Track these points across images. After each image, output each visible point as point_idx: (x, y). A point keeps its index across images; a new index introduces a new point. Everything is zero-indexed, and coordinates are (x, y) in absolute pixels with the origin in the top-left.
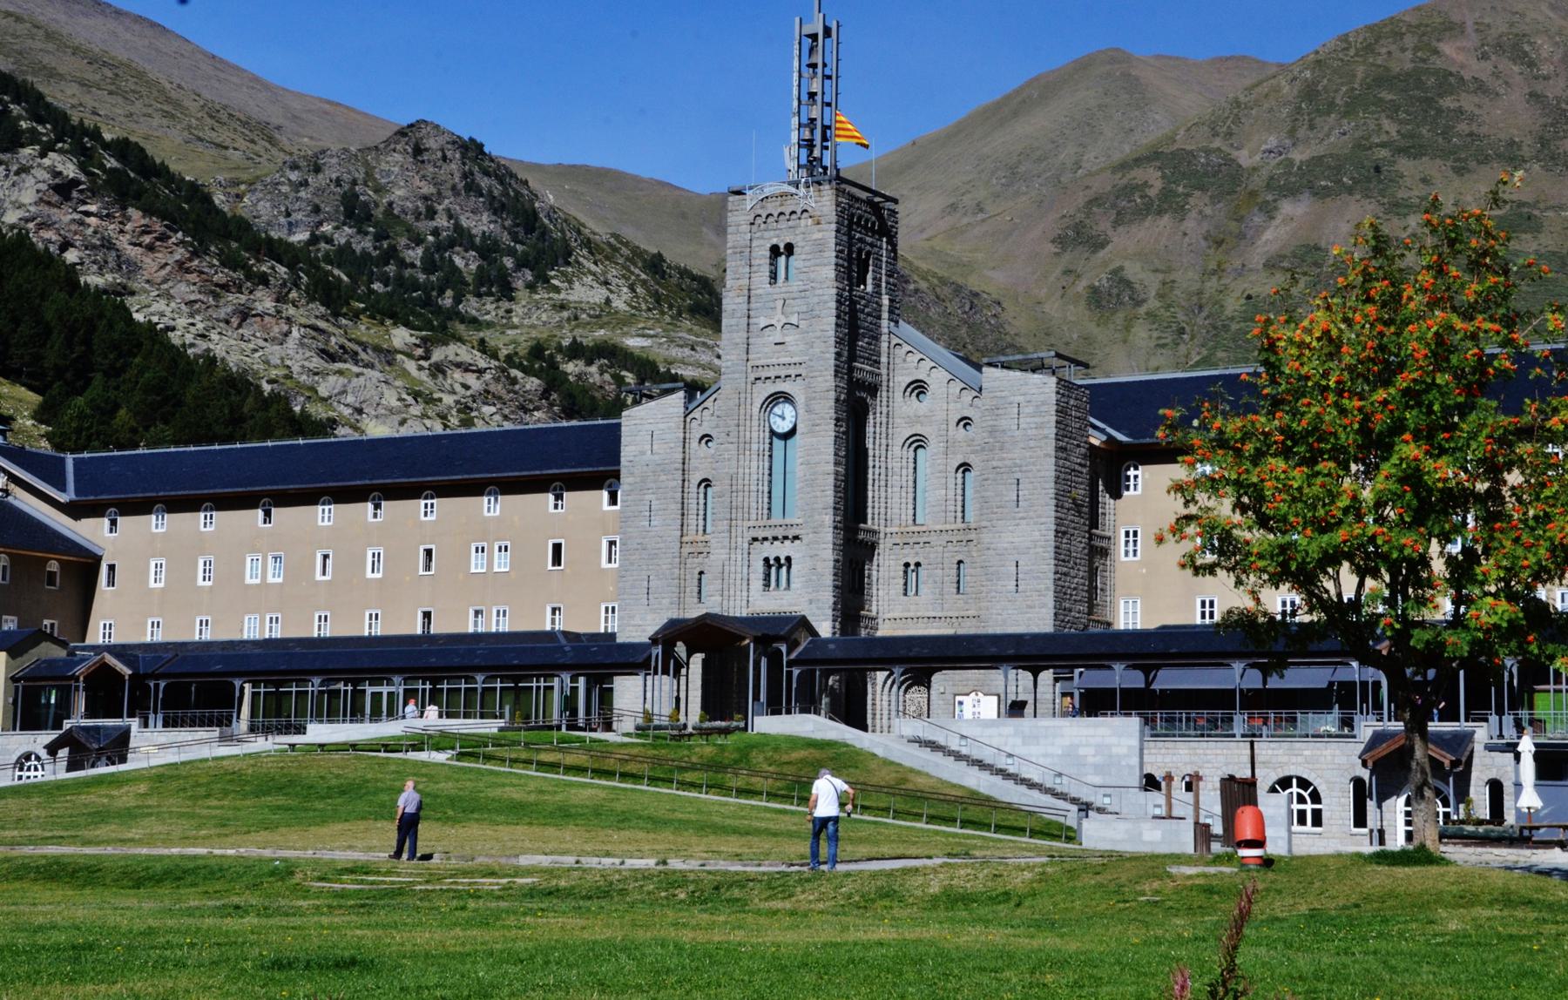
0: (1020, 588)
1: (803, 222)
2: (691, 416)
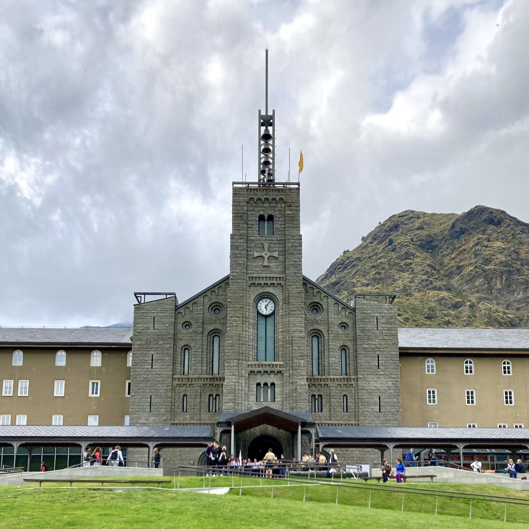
0: (382, 410)
1: (279, 205)
2: (178, 311)
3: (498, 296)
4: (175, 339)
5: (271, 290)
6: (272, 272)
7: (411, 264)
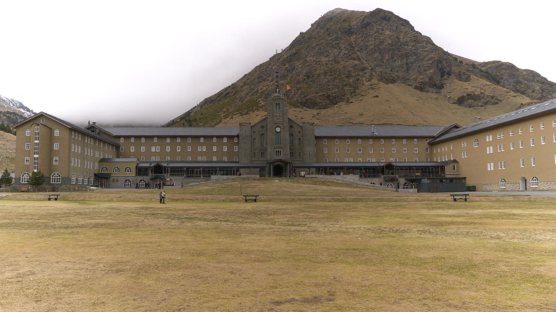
3: (386, 64)
4: (251, 136)
5: (279, 125)
6: (280, 120)
7: (339, 43)
